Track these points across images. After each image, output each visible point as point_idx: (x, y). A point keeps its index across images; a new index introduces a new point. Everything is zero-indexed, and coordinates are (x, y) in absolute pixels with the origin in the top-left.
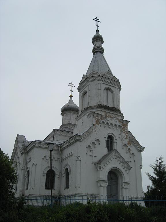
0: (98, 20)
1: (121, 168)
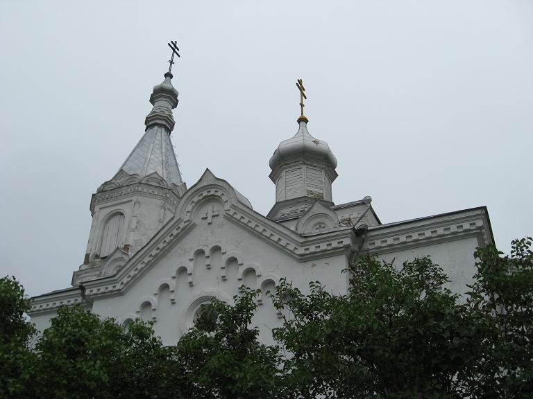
0: (176, 50)
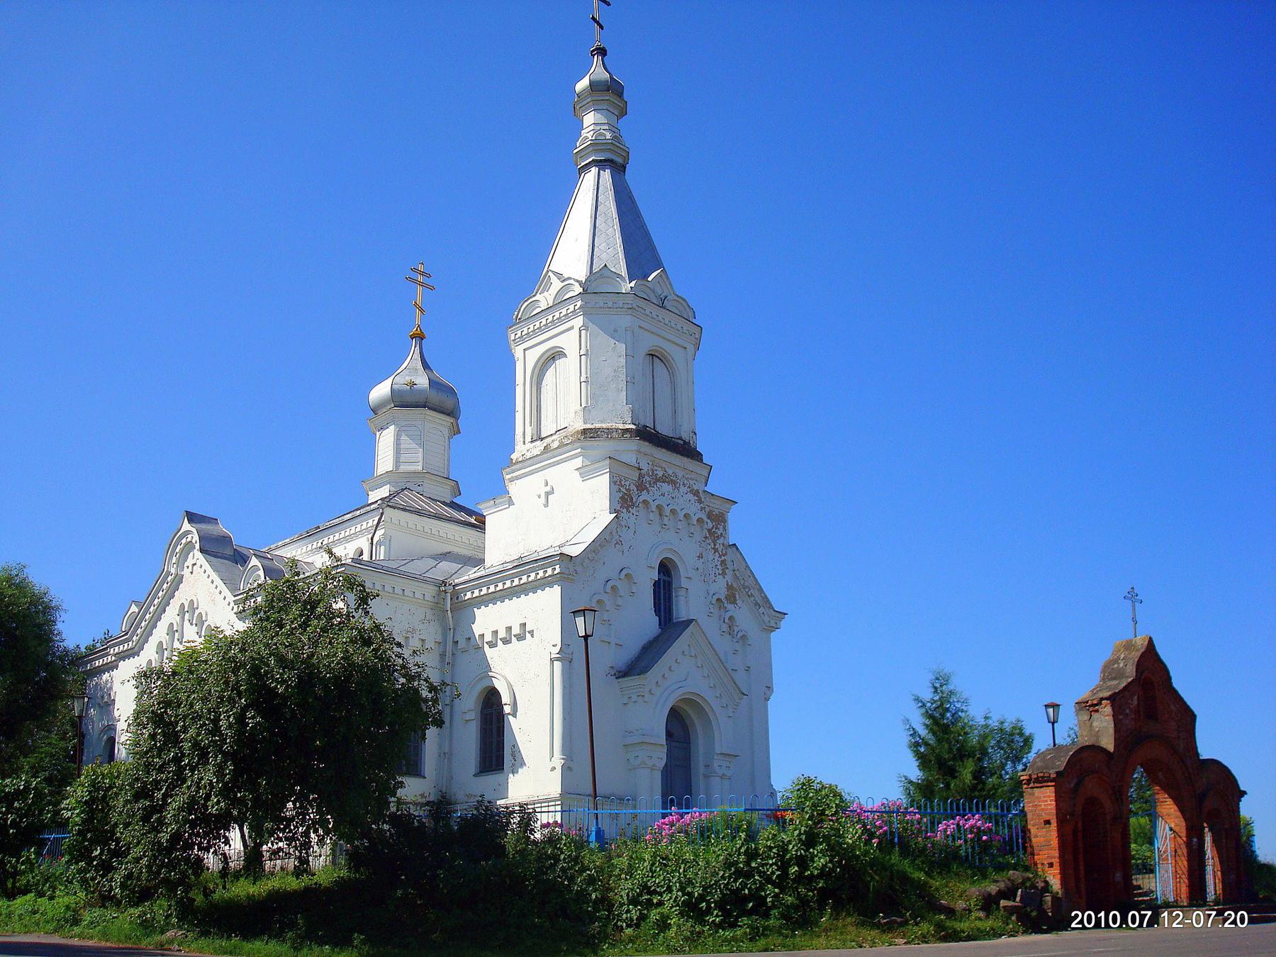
1: (669, 555)
